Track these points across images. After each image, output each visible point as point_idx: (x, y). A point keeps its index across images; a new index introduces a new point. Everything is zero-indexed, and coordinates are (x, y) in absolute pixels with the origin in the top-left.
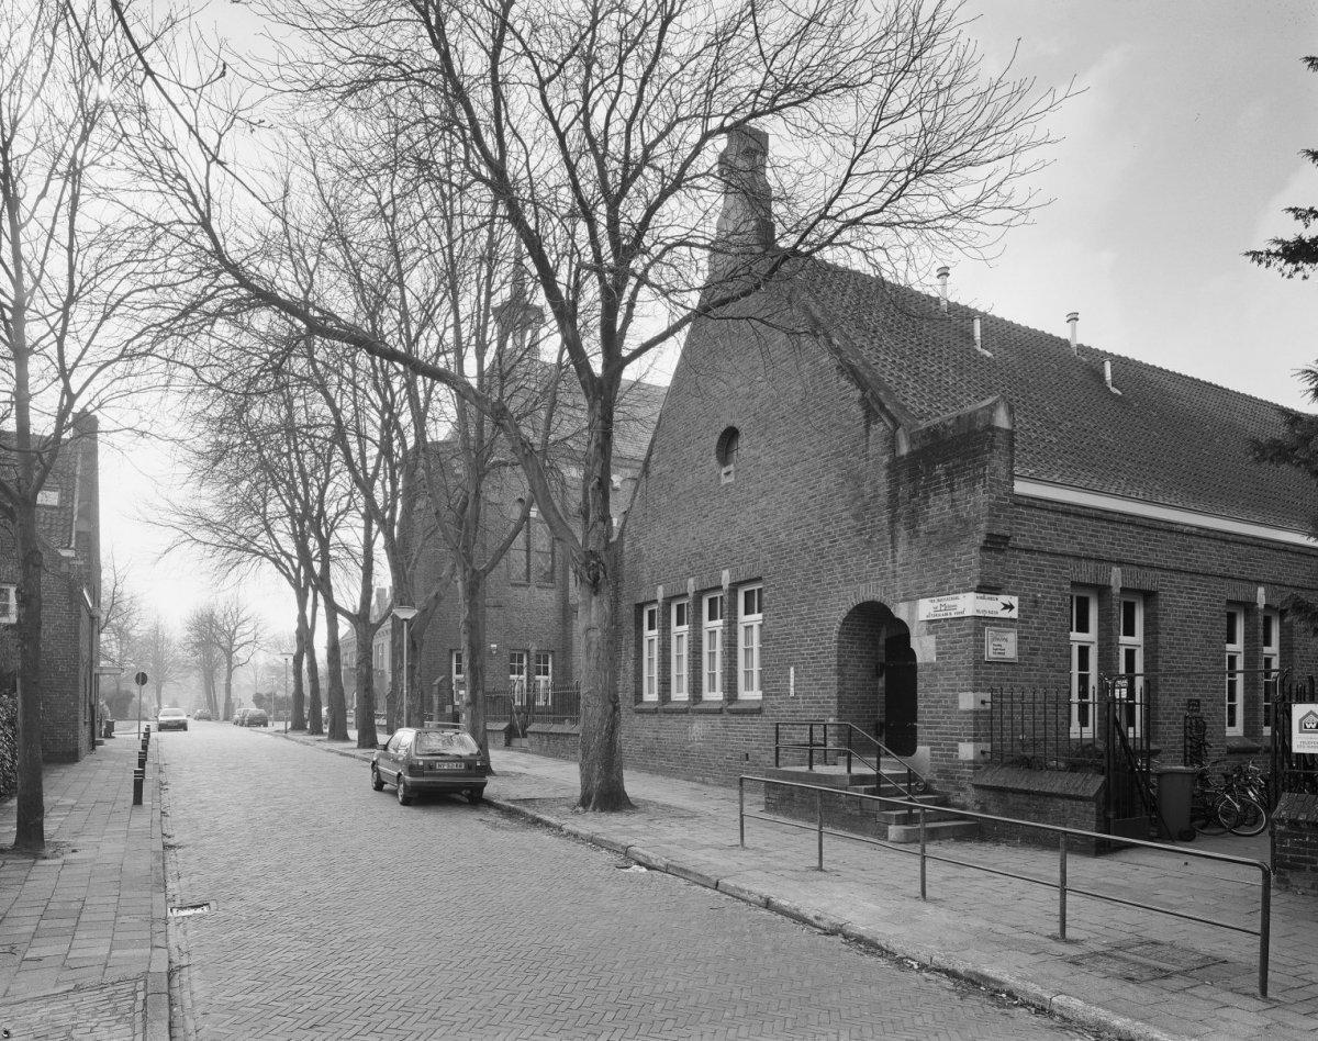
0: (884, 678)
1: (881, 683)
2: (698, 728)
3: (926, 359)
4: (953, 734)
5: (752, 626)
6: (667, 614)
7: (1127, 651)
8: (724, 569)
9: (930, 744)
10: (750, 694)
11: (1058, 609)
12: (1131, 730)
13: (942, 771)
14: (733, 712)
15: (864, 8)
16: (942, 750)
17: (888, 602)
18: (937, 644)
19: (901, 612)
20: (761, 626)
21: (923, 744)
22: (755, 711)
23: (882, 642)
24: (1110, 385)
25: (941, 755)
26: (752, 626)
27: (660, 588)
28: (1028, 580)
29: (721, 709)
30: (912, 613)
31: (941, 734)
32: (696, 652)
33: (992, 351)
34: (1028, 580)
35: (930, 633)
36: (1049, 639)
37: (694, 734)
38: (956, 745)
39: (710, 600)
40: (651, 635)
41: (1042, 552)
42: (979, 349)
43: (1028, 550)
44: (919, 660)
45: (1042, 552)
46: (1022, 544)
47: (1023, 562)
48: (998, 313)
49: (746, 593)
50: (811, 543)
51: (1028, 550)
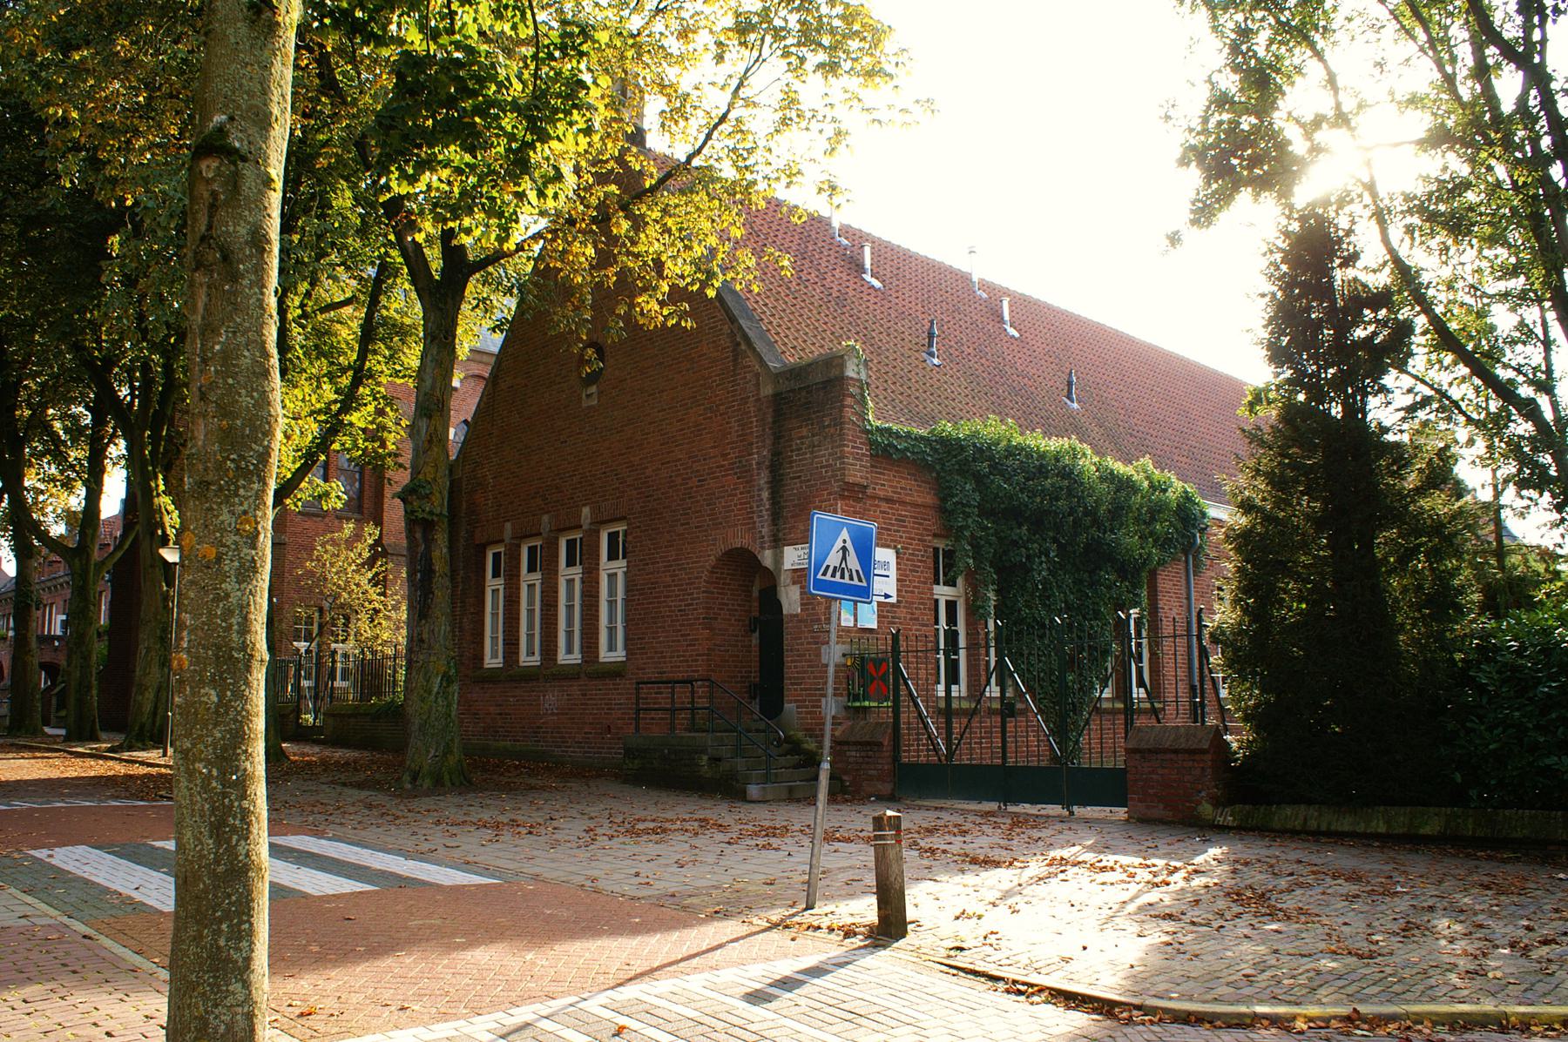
0: (757, 634)
1: (755, 639)
2: (551, 699)
3: (806, 287)
4: (810, 689)
5: (573, 580)
6: (552, 546)
7: (947, 602)
8: (584, 505)
9: (796, 701)
10: (611, 653)
11: (921, 561)
12: (954, 688)
13: (806, 730)
14: (590, 677)
15: (10, 920)
16: (807, 707)
17: (755, 548)
18: (801, 594)
19: (767, 558)
20: (625, 573)
21: (791, 702)
22: (614, 673)
23: (755, 593)
24: (1007, 327)
25: (807, 713)
26: (573, 580)
27: (508, 526)
28: (890, 530)
29: (578, 674)
30: (778, 559)
31: (806, 689)
32: (549, 605)
33: (883, 282)
34: (890, 530)
35: (794, 583)
36: (913, 592)
37: (547, 706)
38: (820, 701)
39: (530, 548)
40: (494, 585)
41: (903, 503)
42: (868, 277)
43: (888, 500)
44: (785, 612)
45: (903, 503)
46: (882, 494)
47: (884, 512)
48: (886, 237)
49: (609, 534)
50: (679, 481)
51: (888, 500)
